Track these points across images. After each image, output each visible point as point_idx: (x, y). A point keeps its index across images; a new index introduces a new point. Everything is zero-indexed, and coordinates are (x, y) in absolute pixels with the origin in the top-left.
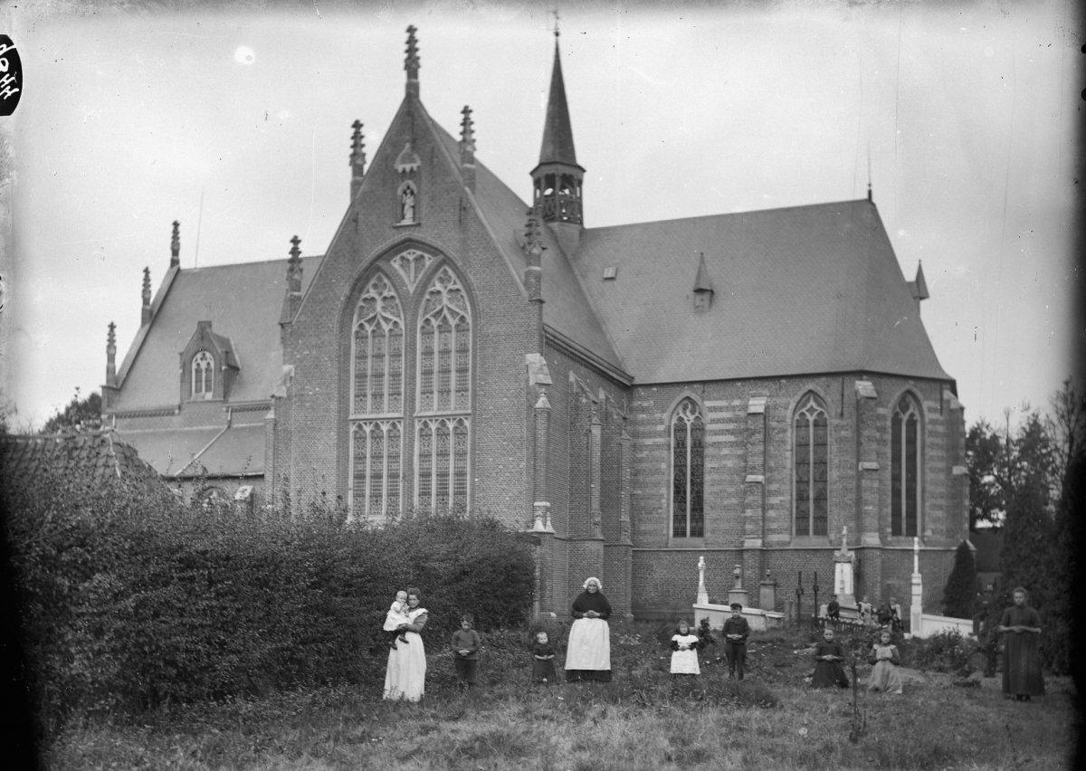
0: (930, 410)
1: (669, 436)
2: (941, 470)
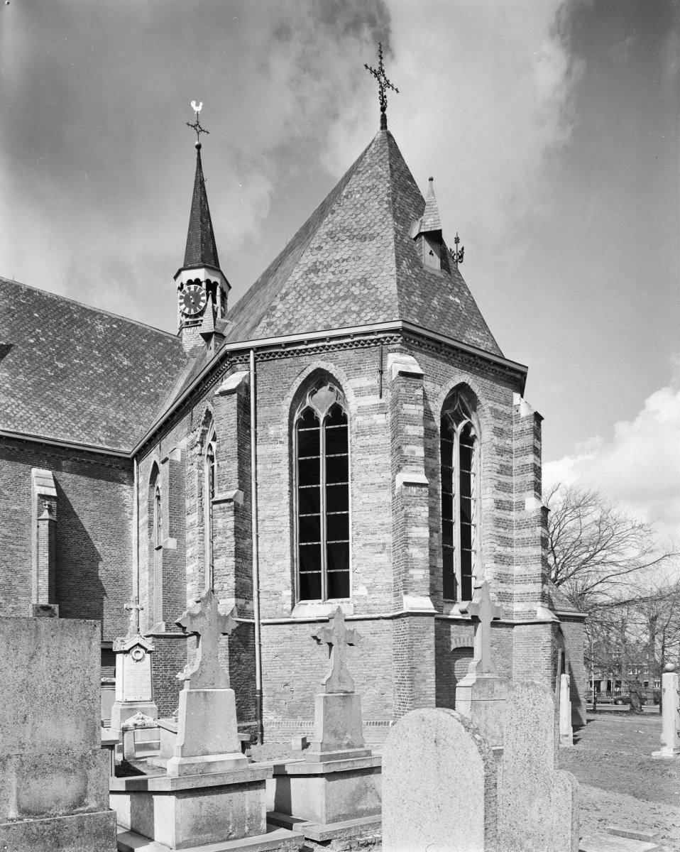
0: (359, 392)
2: (382, 487)
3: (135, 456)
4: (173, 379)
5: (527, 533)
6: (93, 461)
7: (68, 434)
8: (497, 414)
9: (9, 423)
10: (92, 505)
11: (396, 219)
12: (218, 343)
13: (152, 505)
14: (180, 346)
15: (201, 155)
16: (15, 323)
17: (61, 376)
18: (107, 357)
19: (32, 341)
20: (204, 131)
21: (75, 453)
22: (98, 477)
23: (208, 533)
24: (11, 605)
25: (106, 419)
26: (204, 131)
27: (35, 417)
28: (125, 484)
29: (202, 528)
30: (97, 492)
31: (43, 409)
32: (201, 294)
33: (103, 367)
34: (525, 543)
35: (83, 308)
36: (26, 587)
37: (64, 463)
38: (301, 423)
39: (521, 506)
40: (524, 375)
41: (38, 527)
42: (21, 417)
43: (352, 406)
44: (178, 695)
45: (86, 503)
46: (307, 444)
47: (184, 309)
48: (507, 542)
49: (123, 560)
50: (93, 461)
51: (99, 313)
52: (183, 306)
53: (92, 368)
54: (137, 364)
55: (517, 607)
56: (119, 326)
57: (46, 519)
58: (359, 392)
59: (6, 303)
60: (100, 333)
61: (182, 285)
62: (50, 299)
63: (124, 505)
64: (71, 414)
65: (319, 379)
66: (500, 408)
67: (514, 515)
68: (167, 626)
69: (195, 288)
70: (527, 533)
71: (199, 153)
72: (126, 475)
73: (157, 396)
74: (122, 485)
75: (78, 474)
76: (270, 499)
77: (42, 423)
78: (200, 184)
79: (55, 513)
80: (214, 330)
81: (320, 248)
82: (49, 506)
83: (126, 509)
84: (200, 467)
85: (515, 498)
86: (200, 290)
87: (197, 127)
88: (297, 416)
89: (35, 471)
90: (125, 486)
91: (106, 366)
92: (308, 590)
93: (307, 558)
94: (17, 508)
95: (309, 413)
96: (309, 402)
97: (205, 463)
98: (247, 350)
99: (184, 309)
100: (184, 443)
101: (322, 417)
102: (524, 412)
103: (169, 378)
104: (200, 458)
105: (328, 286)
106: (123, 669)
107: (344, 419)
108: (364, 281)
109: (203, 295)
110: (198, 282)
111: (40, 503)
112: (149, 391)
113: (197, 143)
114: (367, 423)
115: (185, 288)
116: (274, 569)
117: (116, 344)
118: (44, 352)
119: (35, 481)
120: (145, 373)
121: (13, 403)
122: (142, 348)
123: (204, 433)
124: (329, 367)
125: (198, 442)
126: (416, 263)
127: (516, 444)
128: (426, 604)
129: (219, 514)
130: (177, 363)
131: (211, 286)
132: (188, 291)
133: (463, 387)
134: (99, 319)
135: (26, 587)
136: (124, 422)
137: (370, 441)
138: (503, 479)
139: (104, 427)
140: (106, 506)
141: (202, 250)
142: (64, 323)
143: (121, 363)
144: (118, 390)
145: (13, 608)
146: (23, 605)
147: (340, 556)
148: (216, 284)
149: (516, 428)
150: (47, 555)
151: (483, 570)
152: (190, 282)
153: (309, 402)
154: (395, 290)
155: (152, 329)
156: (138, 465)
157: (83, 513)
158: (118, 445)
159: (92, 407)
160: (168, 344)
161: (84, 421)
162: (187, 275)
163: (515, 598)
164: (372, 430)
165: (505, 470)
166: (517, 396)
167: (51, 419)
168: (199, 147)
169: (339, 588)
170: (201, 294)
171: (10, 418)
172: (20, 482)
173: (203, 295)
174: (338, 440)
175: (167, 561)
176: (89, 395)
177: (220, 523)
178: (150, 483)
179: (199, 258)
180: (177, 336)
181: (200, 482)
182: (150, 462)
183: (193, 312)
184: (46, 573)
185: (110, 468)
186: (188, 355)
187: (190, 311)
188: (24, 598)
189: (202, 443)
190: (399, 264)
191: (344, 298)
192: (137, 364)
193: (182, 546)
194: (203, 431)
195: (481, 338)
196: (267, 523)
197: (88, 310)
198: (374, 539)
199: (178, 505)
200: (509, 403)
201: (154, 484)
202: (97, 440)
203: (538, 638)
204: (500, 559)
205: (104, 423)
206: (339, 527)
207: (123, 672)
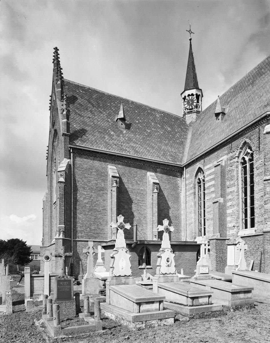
1: (195, 188)
3: (185, 166)
4: (186, 135)
6: (168, 169)
7: (159, 158)
9: (139, 154)
10: (168, 187)
12: (223, 117)
13: (195, 186)
14: (185, 122)
15: (192, 43)
16: (130, 115)
17: (150, 135)
18: (162, 128)
19: (137, 122)
20: (192, 33)
21: (162, 165)
22: (170, 175)
23: (241, 195)
24: (140, 228)
25: (169, 151)
26: (192, 33)
27: (146, 151)
28: (179, 178)
29: (238, 193)
30: (169, 181)
31: (148, 148)
32: (194, 100)
33: (162, 131)
35: (151, 108)
36: (146, 221)
37: (158, 170)
41: (153, 196)
42: (142, 152)
44: (156, 268)
45: (166, 186)
47: (187, 106)
49: (178, 209)
50: (168, 169)
51: (156, 110)
52: (187, 105)
53: (159, 132)
54: (173, 130)
56: (164, 115)
57: (156, 193)
59: (126, 108)
60: (158, 118)
61: (185, 97)
62: (139, 105)
63: (178, 187)
64: (157, 150)
68: (220, 235)
69: (192, 97)
71: (191, 42)
72: (179, 174)
74: (178, 178)
75: (163, 174)
77: (149, 154)
78: (191, 54)
79: (158, 190)
80: (221, 111)
82: (157, 187)
83: (179, 188)
84: (237, 167)
86: (194, 98)
89: (149, 173)
90: (179, 179)
91: (163, 131)
94: (142, 188)
97: (239, 165)
99: (187, 106)
100: (225, 158)
103: (184, 135)
104: (237, 163)
106: (235, 252)
109: (195, 100)
110: (192, 95)
111: (153, 186)
112: (179, 140)
113: (190, 38)
115: (187, 98)
117: (164, 122)
118: (142, 126)
119: (150, 179)
120: (176, 133)
121: (138, 146)
122: (173, 123)
125: (236, 157)
129: (267, 185)
130: (186, 129)
131: (198, 96)
132: (188, 99)
134: (157, 112)
135: (146, 221)
136: (175, 152)
139: (169, 155)
140: (172, 187)
141: (194, 82)
142: (146, 114)
143: (168, 129)
144: (169, 140)
145: (141, 229)
146: (145, 228)
148: (199, 95)
150: (157, 207)
152: (189, 95)
155: (175, 115)
156: (186, 169)
157: (164, 190)
158: (176, 162)
159: (163, 147)
161: (162, 153)
167: (151, 152)
168: (190, 40)
170: (194, 100)
171: (138, 152)
172: (143, 178)
173: (195, 100)
175: (220, 208)
176: (161, 142)
178: (195, 177)
179: (192, 85)
180: (183, 118)
181: (237, 173)
182: (195, 168)
183: (191, 108)
184: (156, 214)
185: (174, 171)
186: (188, 126)
187: (189, 107)
188: (145, 225)
189: (238, 157)
192: (173, 130)
193: (225, 201)
194: (240, 152)
197: (152, 109)
199: (224, 184)
201: (196, 177)
202: (168, 160)
205: (169, 153)
207: (235, 253)
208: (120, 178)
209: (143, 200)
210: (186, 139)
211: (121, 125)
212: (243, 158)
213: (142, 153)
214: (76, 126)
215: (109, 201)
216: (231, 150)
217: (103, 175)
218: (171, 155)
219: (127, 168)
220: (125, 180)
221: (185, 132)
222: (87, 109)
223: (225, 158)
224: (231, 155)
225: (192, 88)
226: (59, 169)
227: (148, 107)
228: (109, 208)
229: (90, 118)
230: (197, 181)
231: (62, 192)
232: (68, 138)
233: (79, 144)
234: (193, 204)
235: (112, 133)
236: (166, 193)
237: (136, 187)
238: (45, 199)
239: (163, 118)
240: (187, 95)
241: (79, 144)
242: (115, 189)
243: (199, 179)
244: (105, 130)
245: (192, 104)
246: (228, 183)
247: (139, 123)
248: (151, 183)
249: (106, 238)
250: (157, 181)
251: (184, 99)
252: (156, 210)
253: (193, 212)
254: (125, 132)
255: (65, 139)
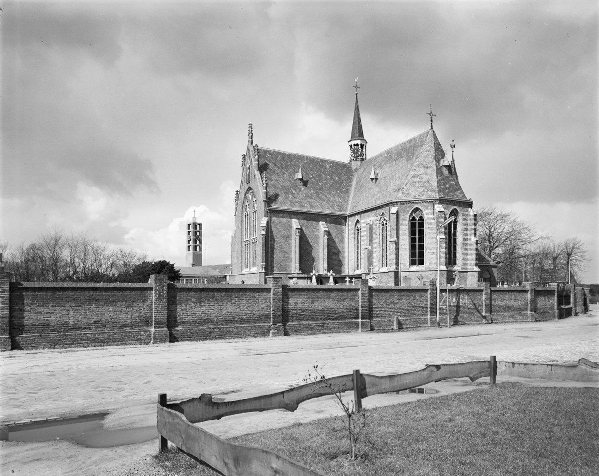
0: (427, 214)
1: (355, 234)
5: (472, 247)
8: (464, 215)
11: (436, 161)
34: (471, 249)
38: (411, 220)
39: (470, 239)
40: (472, 203)
43: (425, 217)
46: (413, 225)
48: (466, 244)
55: (469, 267)
58: (427, 214)
65: (417, 209)
66: (465, 213)
67: (468, 242)
70: (472, 247)
73: (347, 190)
76: (403, 240)
81: (415, 170)
84: (379, 227)
85: (469, 237)
87: (356, 87)
88: (411, 218)
92: (413, 263)
93: (413, 255)
95: (414, 217)
96: (414, 215)
98: (398, 202)
101: (417, 219)
102: (472, 213)
105: (418, 182)
107: (423, 220)
108: (428, 182)
110: (357, 145)
113: (356, 93)
114: (430, 221)
115: (353, 147)
116: (405, 257)
119: (322, 227)
123: (381, 218)
124: (420, 207)
126: (442, 174)
127: (469, 222)
128: (444, 268)
130: (351, 175)
133: (455, 209)
137: (430, 226)
138: (465, 232)
147: (422, 255)
149: (469, 218)
151: (459, 257)
152: (354, 145)
153: (414, 215)
154: (436, 185)
158: (341, 211)
160: (347, 168)
161: (331, 204)
162: (353, 143)
163: (468, 264)
164: (431, 224)
165: (466, 230)
166: (470, 209)
169: (421, 263)
174: (421, 225)
176: (330, 193)
177: (391, 247)
179: (358, 136)
181: (379, 231)
183: (356, 156)
185: (338, 220)
190: (437, 176)
191: (423, 187)
195: (459, 193)
196: (403, 246)
198: (431, 251)
200: (467, 211)
202: (336, 212)
203: (474, 276)
204: (464, 254)
206: (421, 247)
208: (301, 229)
209: (317, 243)
210: (351, 186)
211: (300, 184)
212: (383, 222)
213: (316, 206)
214: (271, 192)
215: (293, 245)
216: (376, 215)
217: (289, 227)
218: (338, 206)
219: (306, 221)
220: (304, 229)
221: (350, 179)
222: (275, 172)
223: (372, 219)
224: (376, 218)
225: (357, 138)
226: (262, 225)
227: (318, 159)
228: (293, 249)
229: (277, 180)
230: (356, 228)
231: (264, 241)
232: (267, 204)
233: (274, 206)
234: (353, 245)
235: (294, 191)
236: (333, 236)
237: (311, 233)
238: (233, 235)
239: (332, 168)
240: (353, 145)
241: (274, 206)
242: (298, 237)
243: (358, 227)
244: (289, 190)
245: (357, 153)
246: (374, 236)
247: (313, 177)
248: (323, 231)
249: (291, 271)
250: (327, 229)
251: (351, 146)
252: (326, 250)
253: (353, 251)
254: (302, 189)
255: (265, 204)
